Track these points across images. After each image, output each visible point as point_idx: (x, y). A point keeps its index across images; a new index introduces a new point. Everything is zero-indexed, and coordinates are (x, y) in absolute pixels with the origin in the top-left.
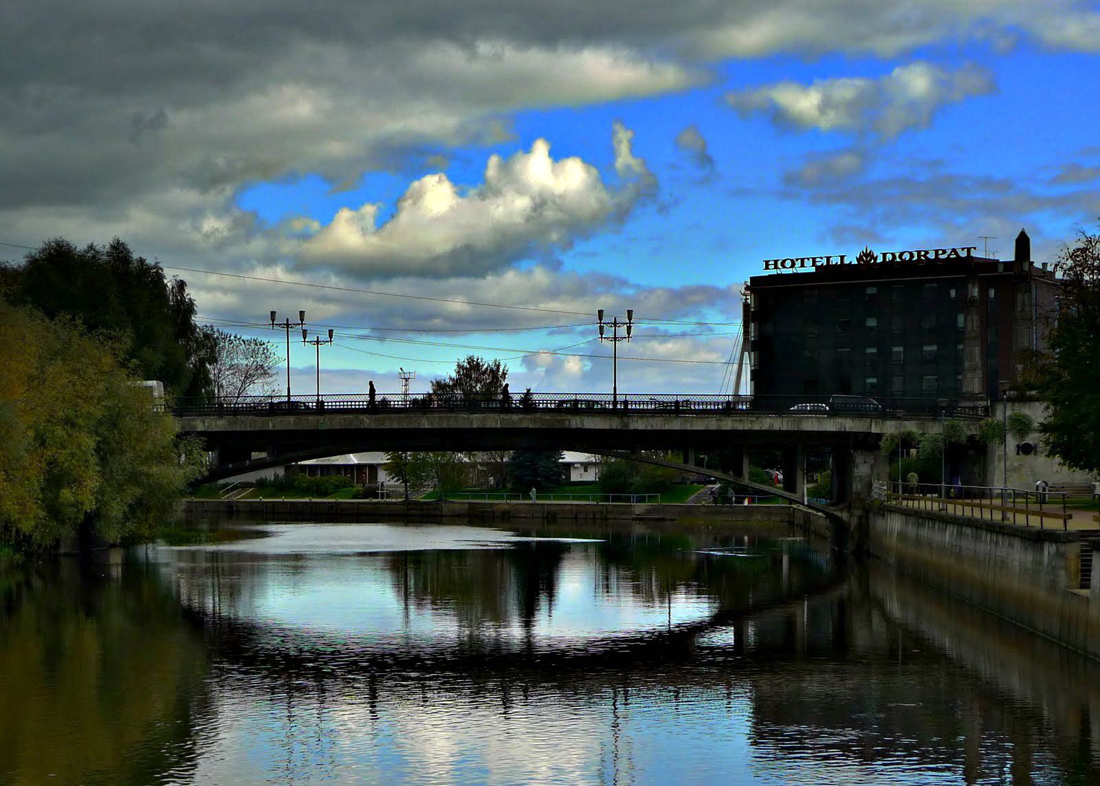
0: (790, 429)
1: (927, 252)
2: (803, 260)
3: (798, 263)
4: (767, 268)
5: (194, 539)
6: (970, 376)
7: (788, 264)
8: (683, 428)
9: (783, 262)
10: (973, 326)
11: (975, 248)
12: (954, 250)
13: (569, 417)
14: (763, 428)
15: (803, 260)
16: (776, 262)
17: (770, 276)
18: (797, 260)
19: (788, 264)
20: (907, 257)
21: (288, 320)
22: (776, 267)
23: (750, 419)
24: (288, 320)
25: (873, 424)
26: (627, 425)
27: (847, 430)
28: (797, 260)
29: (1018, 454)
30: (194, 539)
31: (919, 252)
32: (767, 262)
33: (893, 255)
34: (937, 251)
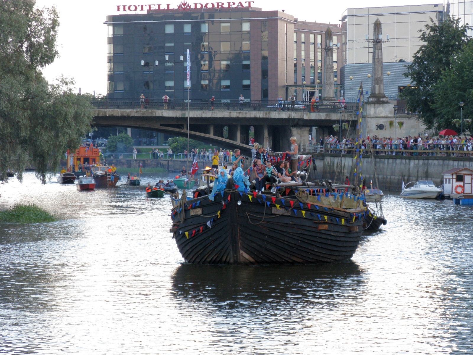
0: (265, 117)
1: (223, 4)
2: (142, 6)
3: (139, 8)
4: (118, 10)
5: (235, 255)
6: (328, 88)
7: (133, 8)
8: (212, 116)
9: (129, 8)
10: (329, 62)
11: (253, 2)
12: (240, 3)
13: (155, 111)
14: (251, 117)
15: (142, 6)
16: (124, 7)
17: (120, 15)
18: (138, 6)
19: (133, 8)
20: (210, 6)
21: (80, 89)
22: (124, 10)
23: (245, 112)
24: (80, 89)
25: (305, 115)
26: (185, 114)
27: (292, 118)
28: (138, 6)
29: (377, 129)
30: (235, 255)
31: (218, 4)
32: (118, 7)
33: (202, 5)
34: (229, 3)
